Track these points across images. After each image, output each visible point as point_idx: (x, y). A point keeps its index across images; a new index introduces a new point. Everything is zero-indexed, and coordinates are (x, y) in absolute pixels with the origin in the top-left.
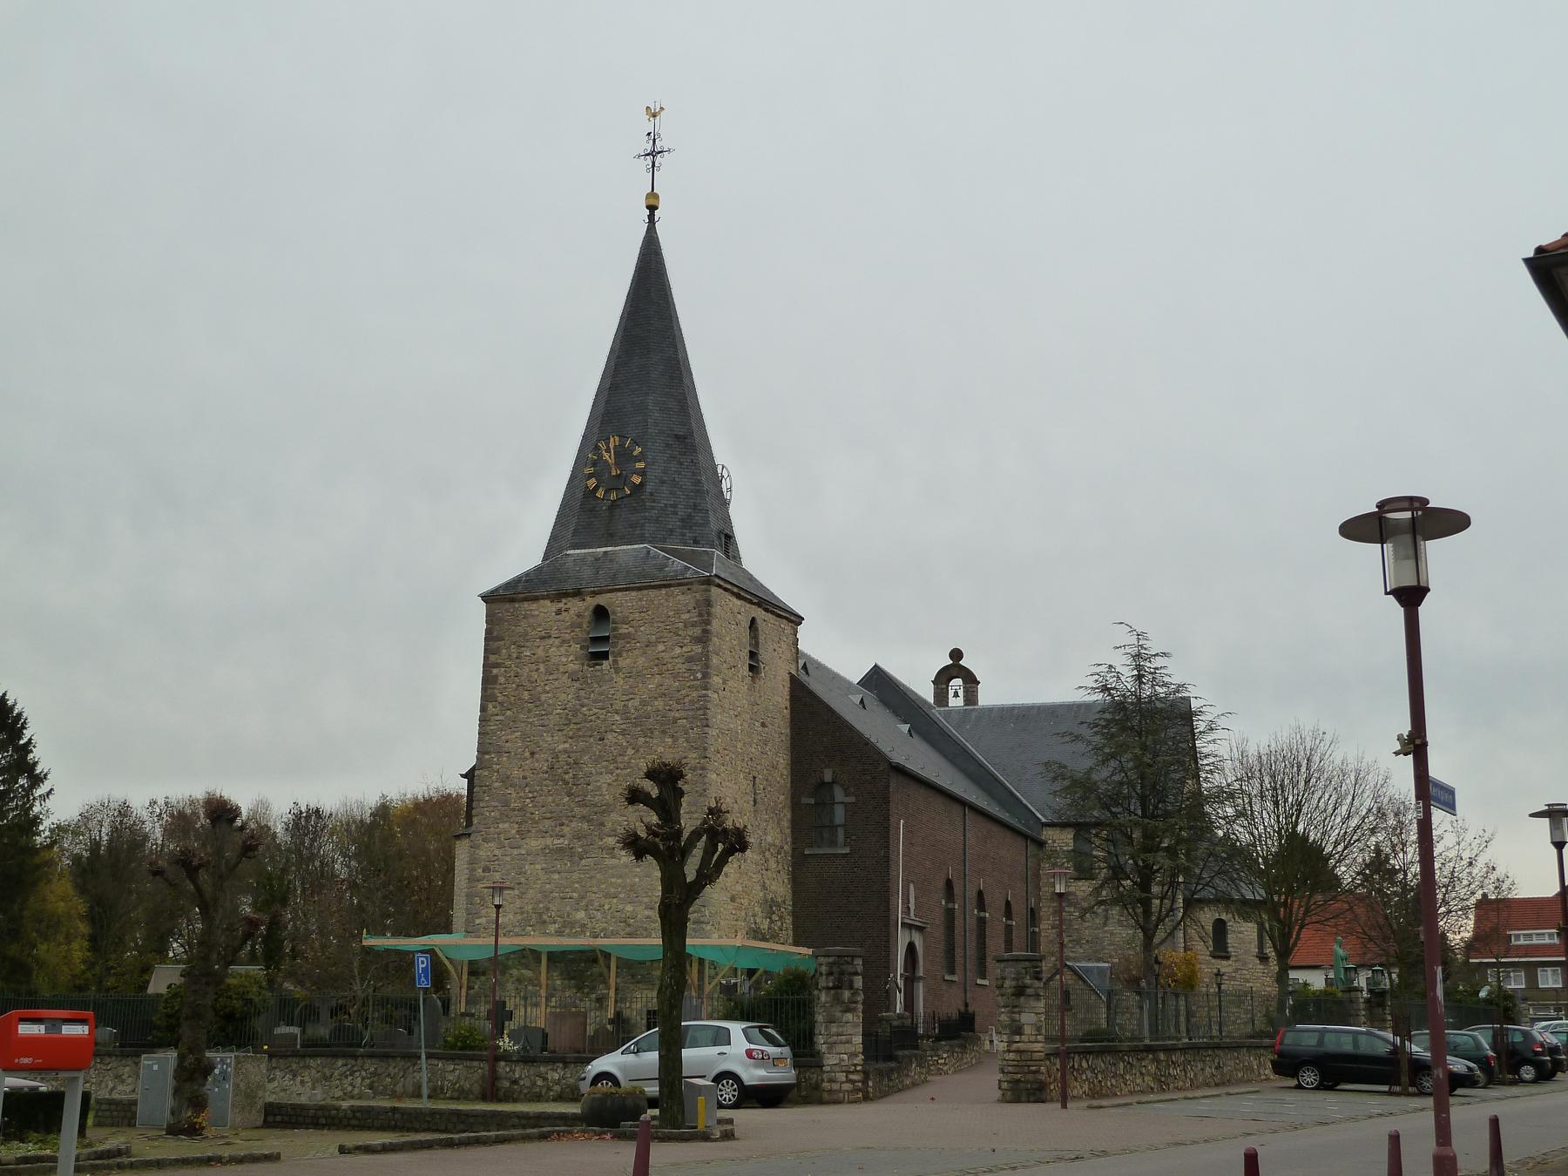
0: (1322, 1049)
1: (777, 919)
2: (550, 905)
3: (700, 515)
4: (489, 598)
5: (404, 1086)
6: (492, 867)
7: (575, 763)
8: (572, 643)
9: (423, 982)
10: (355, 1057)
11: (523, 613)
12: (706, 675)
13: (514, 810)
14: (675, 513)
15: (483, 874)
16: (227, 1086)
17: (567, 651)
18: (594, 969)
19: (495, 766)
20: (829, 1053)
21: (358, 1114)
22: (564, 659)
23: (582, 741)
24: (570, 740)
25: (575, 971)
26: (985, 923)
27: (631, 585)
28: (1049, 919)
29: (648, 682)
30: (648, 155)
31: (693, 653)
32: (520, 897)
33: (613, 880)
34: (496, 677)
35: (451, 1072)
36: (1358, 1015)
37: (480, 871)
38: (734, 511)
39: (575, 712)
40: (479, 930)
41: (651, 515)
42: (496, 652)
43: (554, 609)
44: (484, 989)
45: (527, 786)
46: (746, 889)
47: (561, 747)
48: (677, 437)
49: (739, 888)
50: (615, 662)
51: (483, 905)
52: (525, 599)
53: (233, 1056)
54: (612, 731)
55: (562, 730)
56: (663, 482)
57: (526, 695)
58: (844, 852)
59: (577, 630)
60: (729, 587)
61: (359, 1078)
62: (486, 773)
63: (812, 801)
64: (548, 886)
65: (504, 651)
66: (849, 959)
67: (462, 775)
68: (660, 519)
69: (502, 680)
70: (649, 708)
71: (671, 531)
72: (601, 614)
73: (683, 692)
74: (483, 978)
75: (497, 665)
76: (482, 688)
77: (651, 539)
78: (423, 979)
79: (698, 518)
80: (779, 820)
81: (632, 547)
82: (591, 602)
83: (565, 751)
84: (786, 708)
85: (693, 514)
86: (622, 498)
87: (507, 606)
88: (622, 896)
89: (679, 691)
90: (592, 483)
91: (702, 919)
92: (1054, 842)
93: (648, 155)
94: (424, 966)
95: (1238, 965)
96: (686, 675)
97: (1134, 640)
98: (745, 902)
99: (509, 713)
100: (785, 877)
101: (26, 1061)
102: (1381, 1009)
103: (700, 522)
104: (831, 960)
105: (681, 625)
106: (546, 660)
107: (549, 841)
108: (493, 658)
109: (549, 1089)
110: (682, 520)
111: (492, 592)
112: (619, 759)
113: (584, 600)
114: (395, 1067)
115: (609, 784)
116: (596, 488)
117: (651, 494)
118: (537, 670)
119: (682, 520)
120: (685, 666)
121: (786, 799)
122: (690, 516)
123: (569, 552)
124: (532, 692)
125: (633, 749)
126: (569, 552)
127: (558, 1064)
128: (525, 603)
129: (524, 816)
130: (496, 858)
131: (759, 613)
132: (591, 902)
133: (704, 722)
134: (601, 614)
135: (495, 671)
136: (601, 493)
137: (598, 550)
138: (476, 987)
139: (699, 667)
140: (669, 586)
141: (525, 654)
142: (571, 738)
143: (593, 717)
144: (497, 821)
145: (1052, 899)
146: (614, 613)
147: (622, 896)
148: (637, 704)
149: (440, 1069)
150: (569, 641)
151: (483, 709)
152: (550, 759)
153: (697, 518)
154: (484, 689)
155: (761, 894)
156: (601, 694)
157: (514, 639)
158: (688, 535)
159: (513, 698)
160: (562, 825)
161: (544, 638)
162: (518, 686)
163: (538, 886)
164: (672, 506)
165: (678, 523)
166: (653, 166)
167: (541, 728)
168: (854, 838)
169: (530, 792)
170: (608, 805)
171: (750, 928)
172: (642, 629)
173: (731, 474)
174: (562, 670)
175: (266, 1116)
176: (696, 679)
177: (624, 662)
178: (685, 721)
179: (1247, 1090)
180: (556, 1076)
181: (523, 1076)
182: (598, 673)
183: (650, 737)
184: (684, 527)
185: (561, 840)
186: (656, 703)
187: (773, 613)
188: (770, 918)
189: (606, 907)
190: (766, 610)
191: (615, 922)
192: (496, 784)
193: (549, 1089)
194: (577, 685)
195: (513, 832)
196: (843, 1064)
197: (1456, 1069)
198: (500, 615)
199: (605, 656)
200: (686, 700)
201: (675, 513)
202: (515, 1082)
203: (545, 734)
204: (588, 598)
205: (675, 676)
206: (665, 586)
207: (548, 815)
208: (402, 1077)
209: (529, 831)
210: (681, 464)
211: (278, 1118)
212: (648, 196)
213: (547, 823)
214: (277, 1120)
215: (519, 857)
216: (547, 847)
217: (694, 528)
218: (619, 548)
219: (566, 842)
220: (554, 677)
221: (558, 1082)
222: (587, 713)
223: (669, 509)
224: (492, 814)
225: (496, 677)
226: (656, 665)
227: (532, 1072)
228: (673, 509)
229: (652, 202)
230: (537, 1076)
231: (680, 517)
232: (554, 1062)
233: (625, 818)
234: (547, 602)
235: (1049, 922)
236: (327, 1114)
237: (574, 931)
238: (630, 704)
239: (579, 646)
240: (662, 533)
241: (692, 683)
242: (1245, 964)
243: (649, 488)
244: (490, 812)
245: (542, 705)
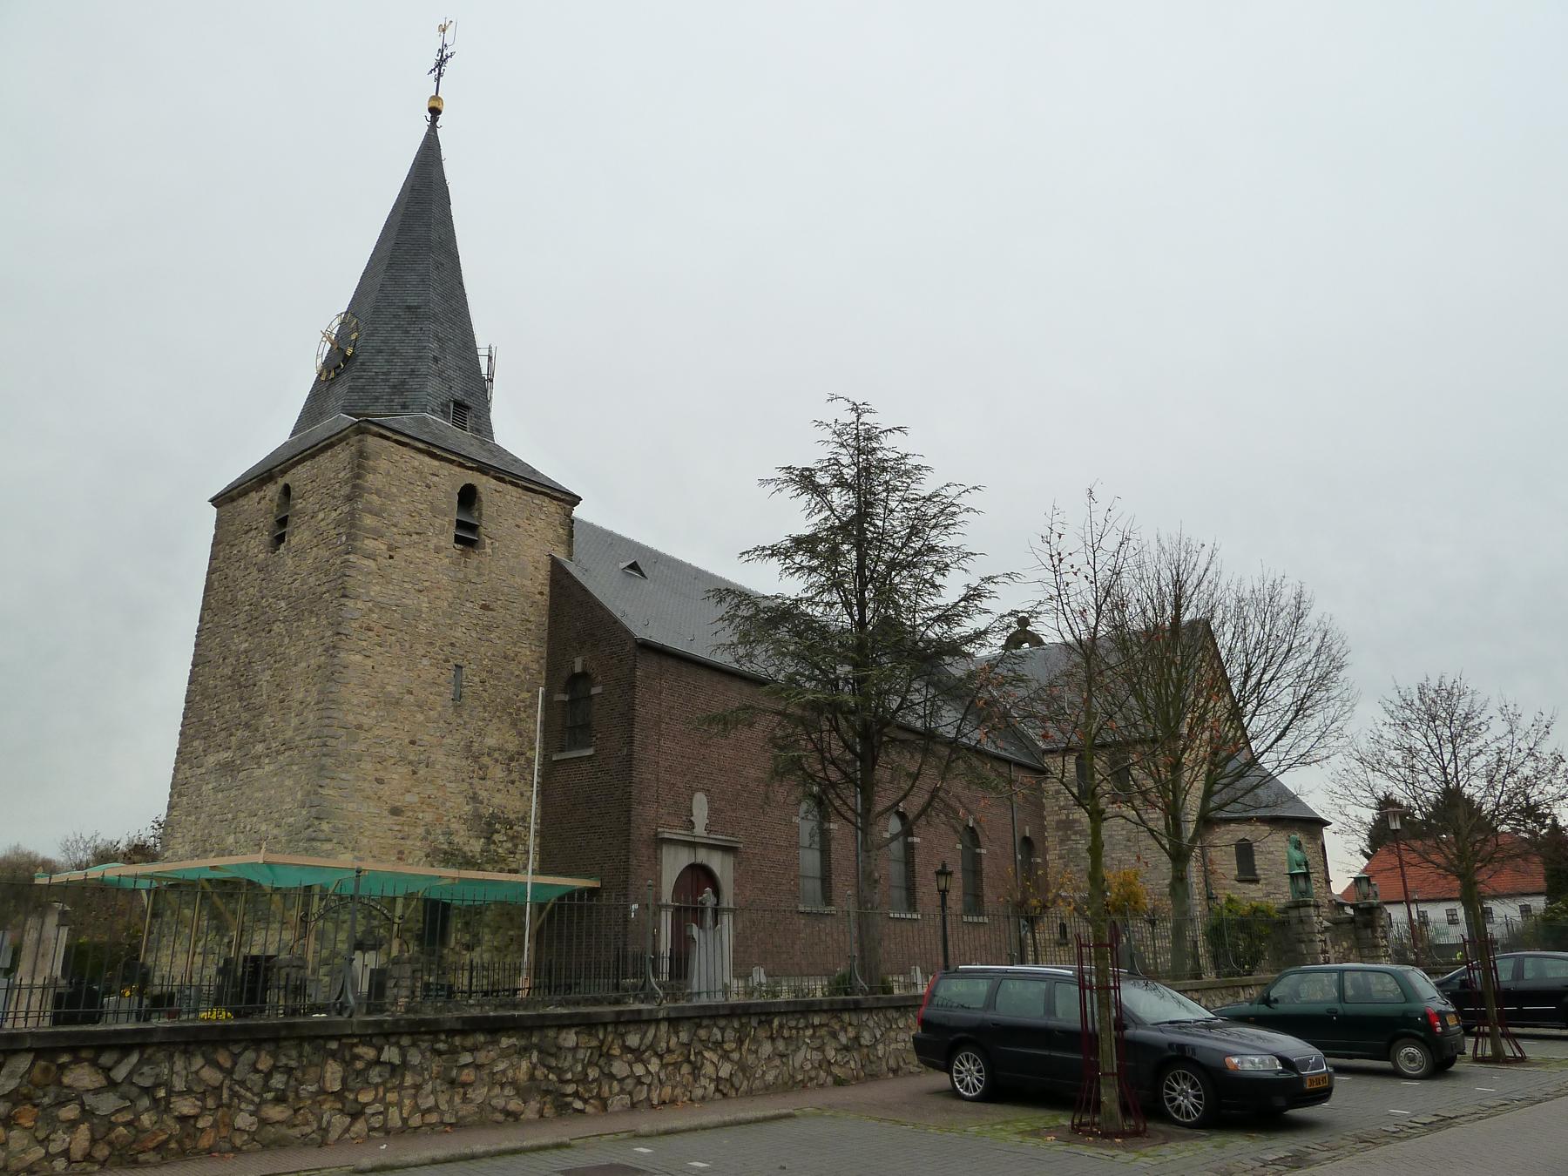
0: (991, 1016)
4: (217, 501)
26: (913, 849)
36: (1312, 941)
48: (409, 308)
63: (566, 698)
71: (377, 398)
79: (413, 383)
84: (541, 593)
95: (1270, 889)
101: (423, 1029)
102: (1369, 931)
117: (362, 364)
122: (404, 382)
131: (484, 484)
145: (1058, 828)
164: (384, 374)
168: (599, 735)
179: (427, 1154)
194: (262, 576)
197: (1248, 1066)
210: (408, 332)
229: (435, 104)
242: (1277, 887)
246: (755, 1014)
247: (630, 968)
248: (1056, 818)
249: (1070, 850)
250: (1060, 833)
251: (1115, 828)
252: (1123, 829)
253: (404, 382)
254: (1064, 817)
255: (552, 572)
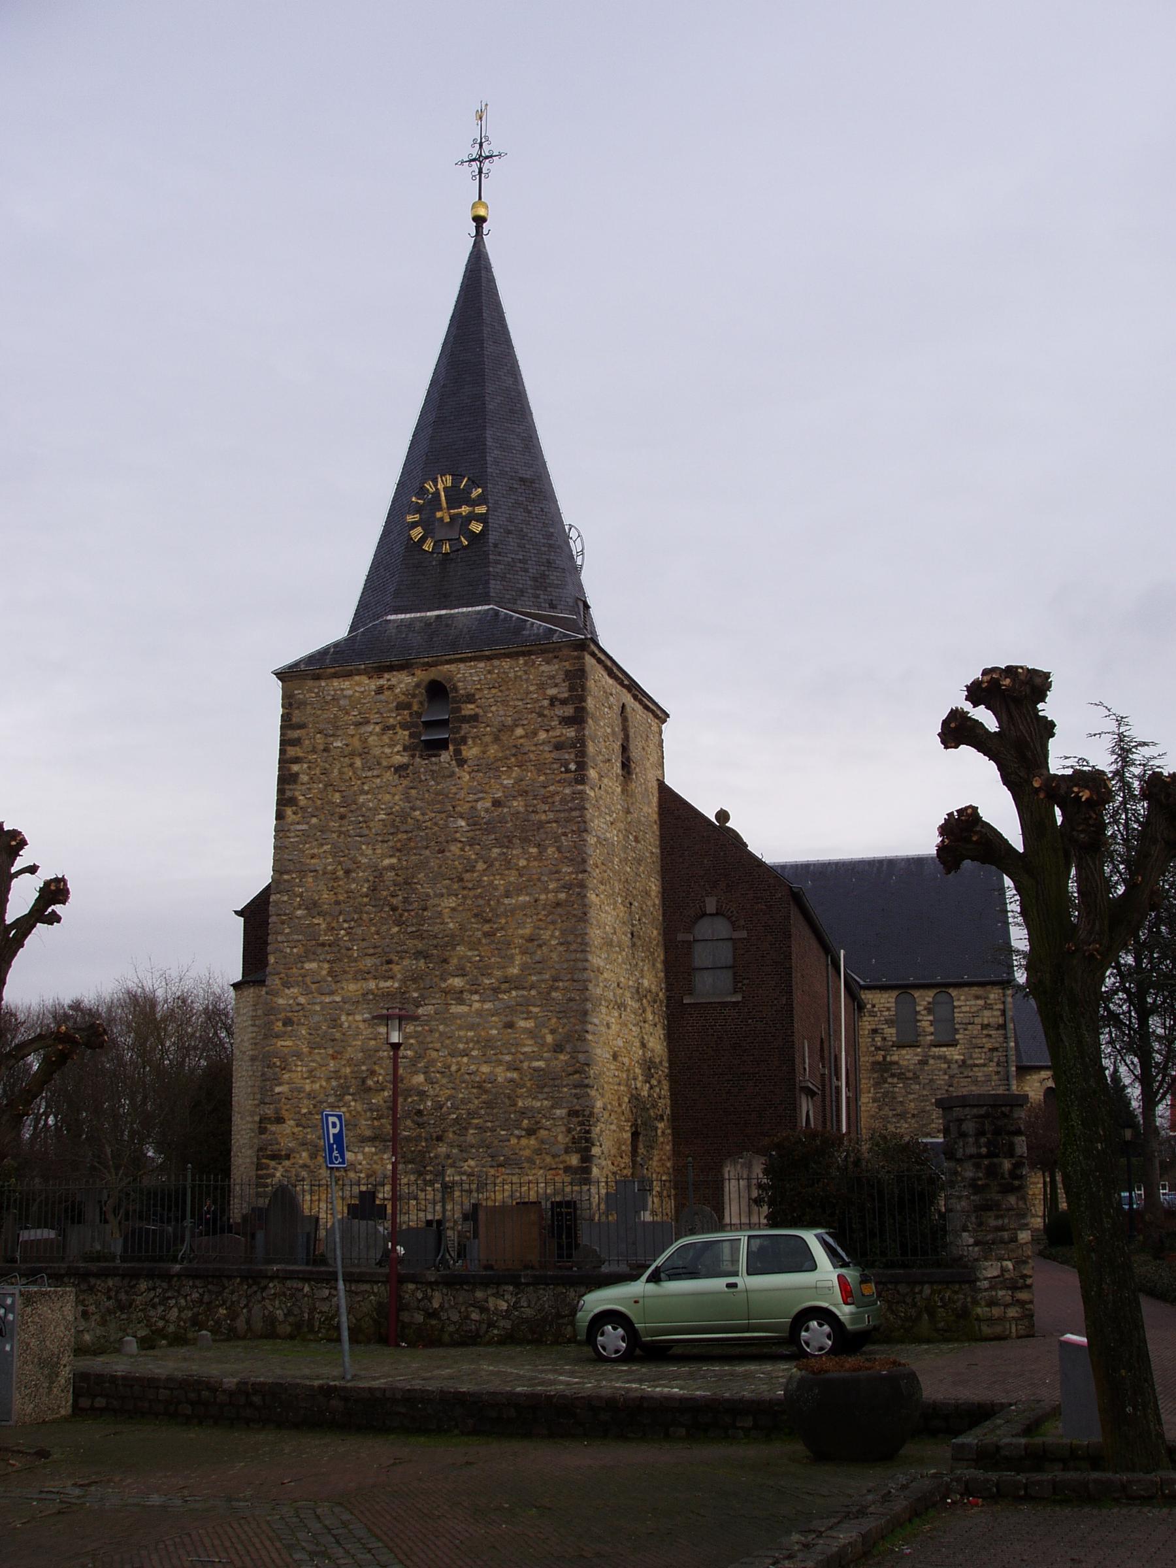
1: (655, 1084)
2: (377, 1068)
3: (555, 573)
4: (283, 675)
5: (248, 1322)
6: (295, 1019)
7: (406, 883)
8: (398, 729)
9: (336, 1158)
10: (167, 1277)
11: (332, 693)
12: (582, 766)
13: (323, 945)
14: (526, 571)
15: (283, 1029)
16: (8, 1348)
17: (391, 739)
18: (439, 1149)
19: (297, 889)
20: (986, 1259)
21: (256, 1399)
22: (388, 750)
23: (415, 854)
24: (398, 854)
25: (413, 1152)
27: (477, 654)
28: (869, 1092)
29: (503, 777)
30: (474, 160)
31: (563, 738)
32: (334, 1058)
33: (462, 1033)
34: (297, 775)
35: (324, 1299)
37: (280, 1024)
38: (586, 578)
39: (404, 816)
40: (280, 1100)
41: (496, 570)
42: (296, 742)
43: (373, 687)
44: (288, 1178)
45: (340, 913)
46: (627, 1045)
47: (387, 862)
49: (620, 1043)
50: (458, 752)
51: (284, 1069)
52: (336, 676)
53: (17, 1292)
54: (456, 840)
55: (387, 842)
56: (509, 532)
57: (337, 798)
58: (734, 1000)
59: (406, 712)
60: (603, 658)
61: (176, 1310)
62: (285, 898)
64: (373, 1042)
65: (307, 742)
66: (1006, 1110)
67: (236, 912)
68: (508, 576)
69: (304, 778)
70: (505, 810)
72: (437, 691)
73: (552, 788)
74: (287, 1163)
75: (297, 760)
76: (278, 790)
77: (497, 599)
78: (335, 1153)
80: (655, 960)
81: (474, 609)
82: (421, 676)
83: (392, 867)
85: (547, 573)
86: (458, 550)
87: (310, 683)
88: (474, 1053)
89: (545, 787)
90: (417, 533)
91: (586, 1081)
92: (874, 1006)
93: (474, 160)
94: (336, 1130)
96: (555, 766)
97: (1112, 726)
98: (626, 1060)
99: (314, 820)
100: (660, 1032)
103: (556, 582)
104: (982, 1111)
105: (546, 703)
106: (364, 753)
107: (372, 985)
108: (292, 751)
109: (491, 1325)
110: (535, 579)
111: (291, 667)
112: (467, 876)
113: (413, 674)
114: (232, 1293)
115: (453, 909)
116: (423, 540)
117: (496, 546)
118: (351, 765)
119: (535, 579)
120: (553, 755)
121: (659, 934)
123: (390, 617)
124: (344, 794)
125: (485, 863)
126: (390, 617)
127: (506, 1288)
128: (335, 680)
129: (339, 951)
130: (300, 1007)
132: (433, 1062)
133: (582, 825)
134: (437, 691)
135: (295, 768)
136: (428, 546)
137: (429, 614)
138: (278, 1174)
139: (573, 756)
140: (530, 653)
141: (335, 745)
142: (399, 850)
143: (429, 824)
144: (301, 959)
145: (873, 1070)
146: (456, 689)
147: (474, 1053)
148: (488, 804)
149: (305, 1296)
150: (393, 727)
151: (280, 816)
152: (371, 878)
153: (551, 577)
154: (280, 791)
155: (641, 1052)
156: (438, 794)
157: (321, 726)
158: (542, 596)
159: (319, 802)
160: (389, 962)
161: (361, 724)
162: (326, 786)
163: (359, 1043)
164: (520, 561)
165: (529, 583)
166: (480, 172)
167: (357, 838)
168: (745, 982)
169: (345, 921)
170: (453, 936)
171: (632, 1095)
172: (493, 709)
173: (582, 534)
174: (385, 763)
175: (76, 1396)
176: (568, 771)
177: (471, 752)
178: (554, 825)
180: (504, 1306)
181: (446, 1306)
182: (434, 768)
183: (507, 847)
184: (537, 588)
185: (389, 983)
186: (515, 804)
187: (641, 702)
188: (649, 1083)
189: (454, 1068)
190: (635, 697)
191: (467, 1088)
192: (299, 912)
193: (491, 1325)
195: (324, 972)
196: (1007, 1276)
198: (301, 696)
199: (442, 745)
200: (557, 798)
201: (526, 571)
202: (434, 1314)
203: (364, 847)
204: (418, 672)
205: (540, 768)
206: (523, 654)
207: (371, 951)
208: (246, 1306)
209: (345, 972)
210: (529, 512)
211: (100, 1402)
212: (474, 206)
213: (369, 962)
214: (97, 1405)
215: (331, 1006)
216: (370, 992)
217: (549, 589)
218: (456, 611)
219: (396, 985)
220: (375, 773)
221: (507, 1315)
222: (420, 818)
223: (519, 565)
224: (295, 950)
225: (297, 775)
226: (514, 755)
227: (461, 1300)
228: (522, 565)
230: (472, 1305)
231: (531, 575)
232: (498, 1284)
233: (476, 953)
234: (364, 679)
235: (870, 1095)
236: (192, 1396)
237: (410, 1100)
238: (479, 805)
239: (407, 733)
240: (510, 592)
241: (563, 776)
243: (493, 537)
244: (292, 948)
245: (359, 809)
246: (928, 1282)
247: (197, 1189)
248: (872, 1059)
249: (885, 1094)
250: (875, 1075)
251: (937, 1073)
252: (945, 1074)
253: (544, 576)
254: (881, 1059)
255: (660, 799)
